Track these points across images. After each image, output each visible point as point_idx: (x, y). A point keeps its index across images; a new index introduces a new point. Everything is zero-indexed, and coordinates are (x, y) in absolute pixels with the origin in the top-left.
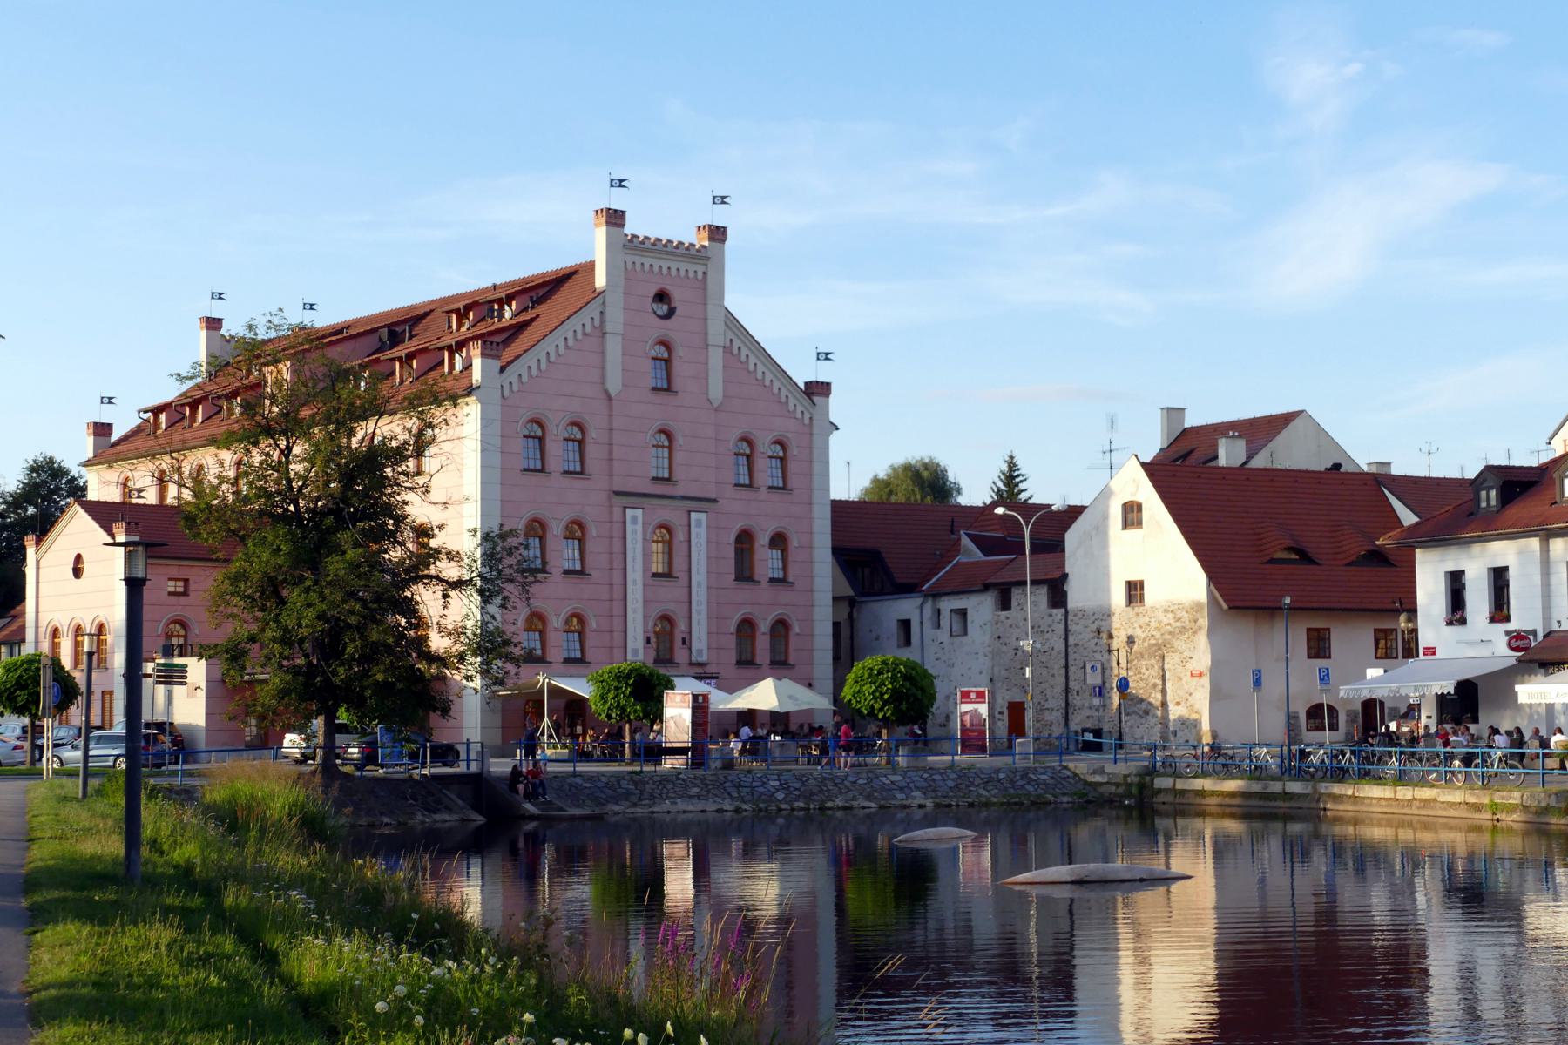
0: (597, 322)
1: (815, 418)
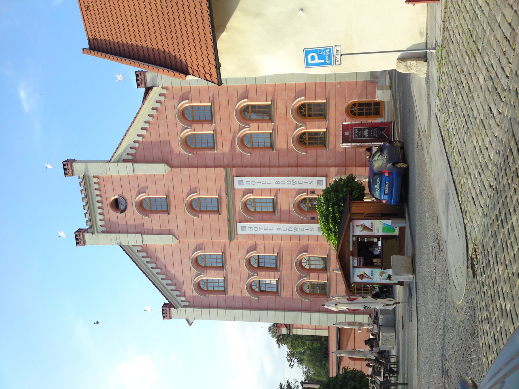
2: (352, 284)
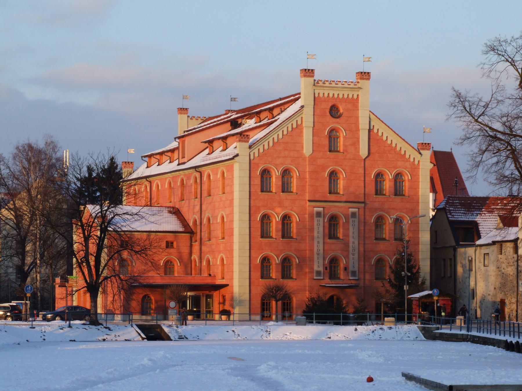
0: (299, 123)
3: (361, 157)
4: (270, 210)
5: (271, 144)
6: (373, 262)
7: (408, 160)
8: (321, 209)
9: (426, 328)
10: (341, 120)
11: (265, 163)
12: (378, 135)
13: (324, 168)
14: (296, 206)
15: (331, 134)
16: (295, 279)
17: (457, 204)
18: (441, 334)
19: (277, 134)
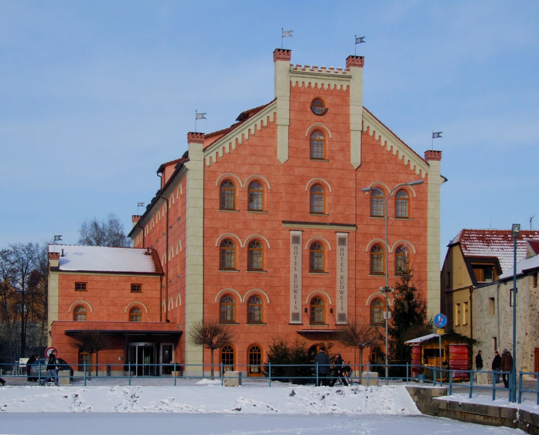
0: (271, 120)
1: (429, 173)
2: (29, 346)
3: (353, 167)
4: (231, 232)
5: (234, 146)
6: (367, 303)
7: (413, 173)
8: (299, 233)
9: (421, 391)
10: (327, 118)
11: (225, 172)
12: (374, 140)
13: (303, 180)
14: (266, 228)
15: (313, 137)
16: (264, 324)
17: (474, 238)
18: (451, 404)
19: (241, 134)
